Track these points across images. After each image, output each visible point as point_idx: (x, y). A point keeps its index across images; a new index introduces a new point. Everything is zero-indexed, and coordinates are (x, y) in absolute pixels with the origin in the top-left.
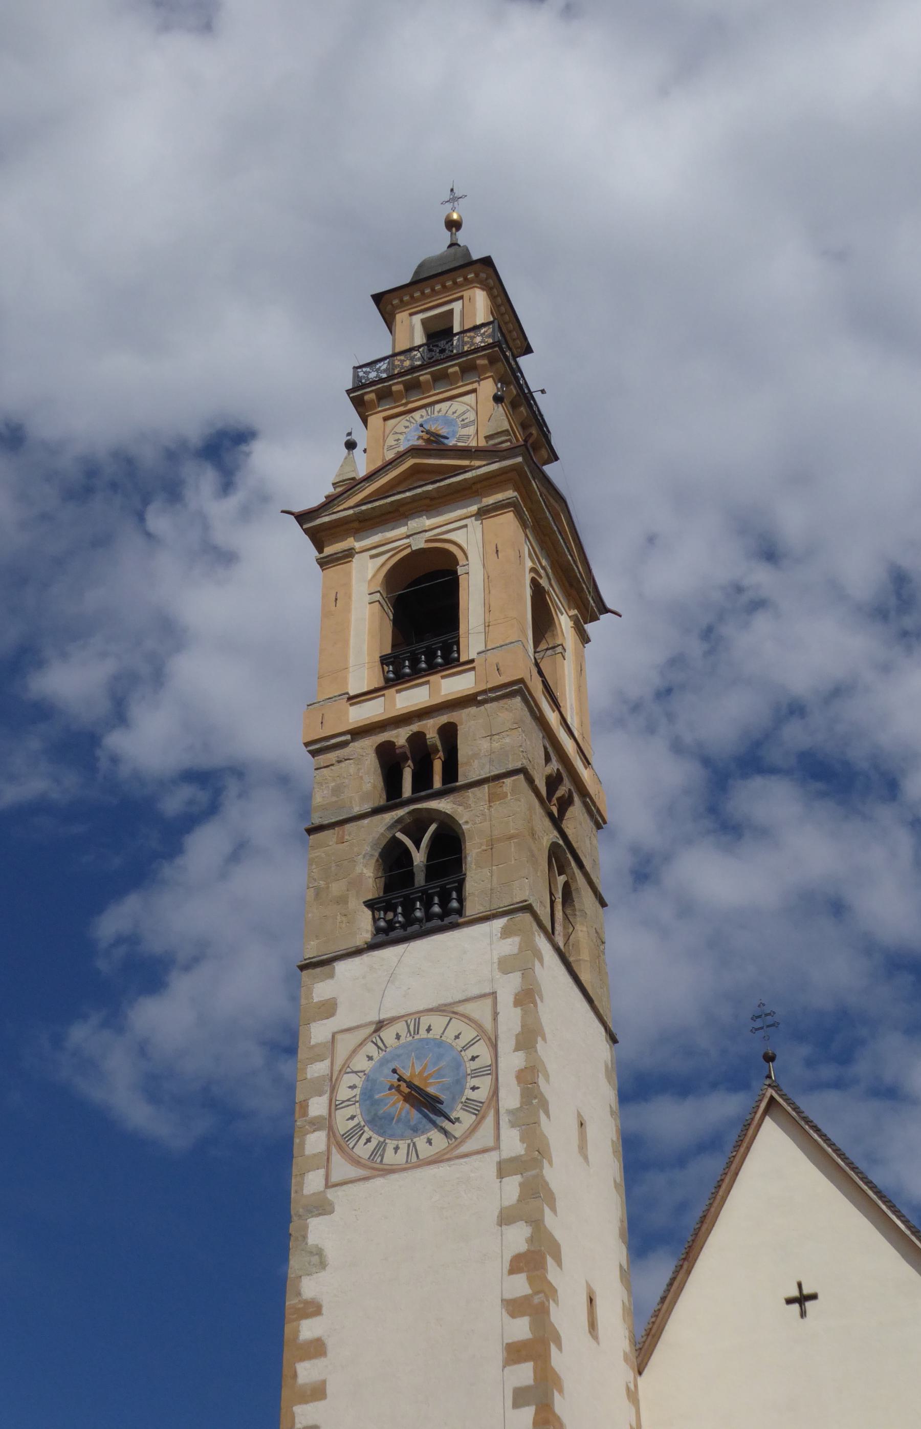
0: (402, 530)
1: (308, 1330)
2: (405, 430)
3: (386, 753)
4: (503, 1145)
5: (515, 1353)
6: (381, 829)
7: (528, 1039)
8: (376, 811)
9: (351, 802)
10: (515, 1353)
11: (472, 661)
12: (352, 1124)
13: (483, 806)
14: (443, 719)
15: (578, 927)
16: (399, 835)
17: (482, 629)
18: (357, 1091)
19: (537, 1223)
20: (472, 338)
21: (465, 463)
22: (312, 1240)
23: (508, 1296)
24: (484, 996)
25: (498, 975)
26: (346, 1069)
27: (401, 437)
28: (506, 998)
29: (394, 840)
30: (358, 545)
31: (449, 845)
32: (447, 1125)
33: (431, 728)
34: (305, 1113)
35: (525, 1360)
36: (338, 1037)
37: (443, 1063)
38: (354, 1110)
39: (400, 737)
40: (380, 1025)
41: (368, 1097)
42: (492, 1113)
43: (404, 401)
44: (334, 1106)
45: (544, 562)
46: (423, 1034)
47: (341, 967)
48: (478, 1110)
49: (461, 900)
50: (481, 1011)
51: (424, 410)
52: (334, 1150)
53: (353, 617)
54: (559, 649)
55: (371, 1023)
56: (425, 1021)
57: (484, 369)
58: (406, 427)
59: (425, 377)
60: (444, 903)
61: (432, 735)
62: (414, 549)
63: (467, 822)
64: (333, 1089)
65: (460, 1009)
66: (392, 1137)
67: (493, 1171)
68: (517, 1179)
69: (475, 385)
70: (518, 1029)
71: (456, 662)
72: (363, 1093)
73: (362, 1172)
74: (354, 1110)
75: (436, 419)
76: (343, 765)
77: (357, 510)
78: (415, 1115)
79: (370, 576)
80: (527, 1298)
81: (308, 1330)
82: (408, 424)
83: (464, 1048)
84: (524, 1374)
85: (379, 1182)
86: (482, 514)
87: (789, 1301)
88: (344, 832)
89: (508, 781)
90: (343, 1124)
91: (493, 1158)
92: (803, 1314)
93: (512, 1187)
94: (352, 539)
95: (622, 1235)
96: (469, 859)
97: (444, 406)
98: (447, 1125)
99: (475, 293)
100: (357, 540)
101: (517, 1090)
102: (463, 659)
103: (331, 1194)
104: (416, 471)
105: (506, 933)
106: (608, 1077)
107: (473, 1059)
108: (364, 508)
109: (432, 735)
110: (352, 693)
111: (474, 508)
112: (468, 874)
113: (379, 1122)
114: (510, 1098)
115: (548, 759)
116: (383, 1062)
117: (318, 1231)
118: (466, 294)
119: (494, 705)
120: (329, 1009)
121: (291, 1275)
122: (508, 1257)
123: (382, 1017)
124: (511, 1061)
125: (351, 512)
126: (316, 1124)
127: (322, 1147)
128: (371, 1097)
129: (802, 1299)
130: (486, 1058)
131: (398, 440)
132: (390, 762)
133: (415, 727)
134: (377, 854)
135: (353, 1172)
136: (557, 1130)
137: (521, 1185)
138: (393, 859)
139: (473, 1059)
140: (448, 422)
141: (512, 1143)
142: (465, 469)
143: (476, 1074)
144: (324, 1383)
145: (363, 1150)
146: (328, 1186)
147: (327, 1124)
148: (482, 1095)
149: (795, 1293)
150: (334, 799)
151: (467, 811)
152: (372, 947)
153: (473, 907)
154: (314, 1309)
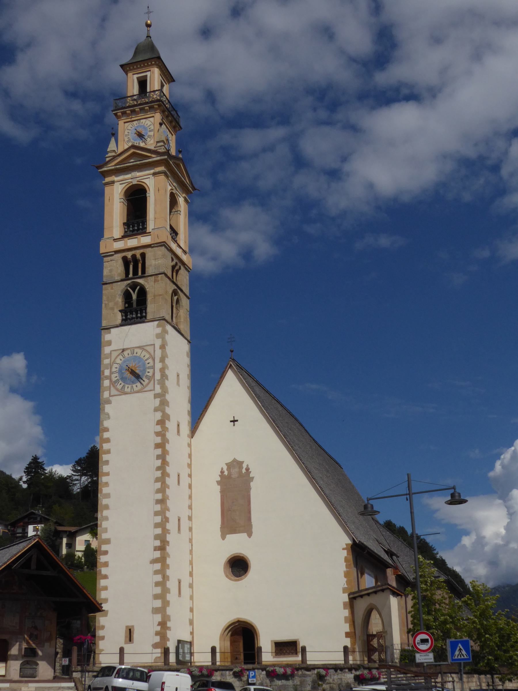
0: (129, 176)
1: (106, 435)
3: (125, 259)
4: (156, 389)
5: (157, 446)
6: (124, 287)
7: (162, 360)
8: (122, 280)
10: (157, 446)
11: (150, 233)
12: (116, 379)
13: (152, 283)
14: (141, 251)
15: (181, 311)
16: (129, 288)
17: (153, 219)
18: (117, 369)
19: (163, 412)
20: (153, 95)
21: (149, 155)
22: (106, 411)
23: (156, 431)
24: (152, 345)
25: (155, 339)
26: (114, 362)
27: (130, 131)
28: (157, 346)
30: (116, 179)
31: (143, 293)
32: (142, 381)
33: (138, 253)
34: (103, 374)
35: (159, 448)
36: (112, 352)
37: (140, 364)
38: (117, 375)
39: (129, 255)
40: (123, 350)
41: (120, 371)
42: (153, 380)
44: (111, 373)
45: (175, 184)
46: (135, 354)
47: (112, 330)
48: (149, 378)
49: (146, 313)
50: (150, 349)
52: (111, 386)
53: (115, 207)
54: (179, 212)
55: (120, 349)
56: (136, 350)
57: (156, 109)
59: (137, 109)
60: (141, 313)
61: (138, 256)
64: (111, 368)
65: (145, 348)
66: (127, 384)
67: (153, 396)
68: (159, 399)
69: (154, 115)
70: (160, 356)
71: (145, 233)
72: (119, 370)
73: (119, 393)
74: (117, 375)
75: (141, 126)
77: (115, 167)
78: (133, 378)
80: (160, 432)
81: (106, 435)
83: (146, 360)
84: (159, 451)
85: (123, 396)
86: (154, 174)
87: (231, 421)
90: (114, 379)
91: (152, 393)
92: (234, 425)
93: (158, 401)
94: (114, 176)
95: (189, 402)
97: (144, 121)
98: (142, 381)
100: (116, 177)
101: (160, 374)
102: (148, 231)
103: (111, 398)
104: (134, 154)
105: (158, 326)
106: (188, 356)
107: (148, 363)
108: (118, 167)
110: (115, 238)
111: (152, 171)
113: (123, 379)
114: (158, 376)
115: (173, 260)
116: (124, 362)
117: (108, 408)
118: (152, 69)
120: (109, 343)
121: (101, 420)
122: (156, 421)
123: (125, 347)
124: (158, 366)
125: (113, 167)
126: (107, 378)
127: (108, 385)
128: (121, 371)
129: (234, 421)
130: (151, 364)
132: (126, 262)
133: (133, 252)
135: (116, 393)
136: (170, 383)
137: (160, 401)
138: (127, 296)
139: (148, 363)
140: (145, 128)
141: (158, 389)
142: (149, 157)
143: (149, 368)
144: (110, 449)
145: (119, 387)
146: (110, 396)
147: (109, 378)
148: (150, 374)
149: (232, 419)
151: (148, 284)
152: (121, 325)
153: (149, 317)
154: (107, 430)
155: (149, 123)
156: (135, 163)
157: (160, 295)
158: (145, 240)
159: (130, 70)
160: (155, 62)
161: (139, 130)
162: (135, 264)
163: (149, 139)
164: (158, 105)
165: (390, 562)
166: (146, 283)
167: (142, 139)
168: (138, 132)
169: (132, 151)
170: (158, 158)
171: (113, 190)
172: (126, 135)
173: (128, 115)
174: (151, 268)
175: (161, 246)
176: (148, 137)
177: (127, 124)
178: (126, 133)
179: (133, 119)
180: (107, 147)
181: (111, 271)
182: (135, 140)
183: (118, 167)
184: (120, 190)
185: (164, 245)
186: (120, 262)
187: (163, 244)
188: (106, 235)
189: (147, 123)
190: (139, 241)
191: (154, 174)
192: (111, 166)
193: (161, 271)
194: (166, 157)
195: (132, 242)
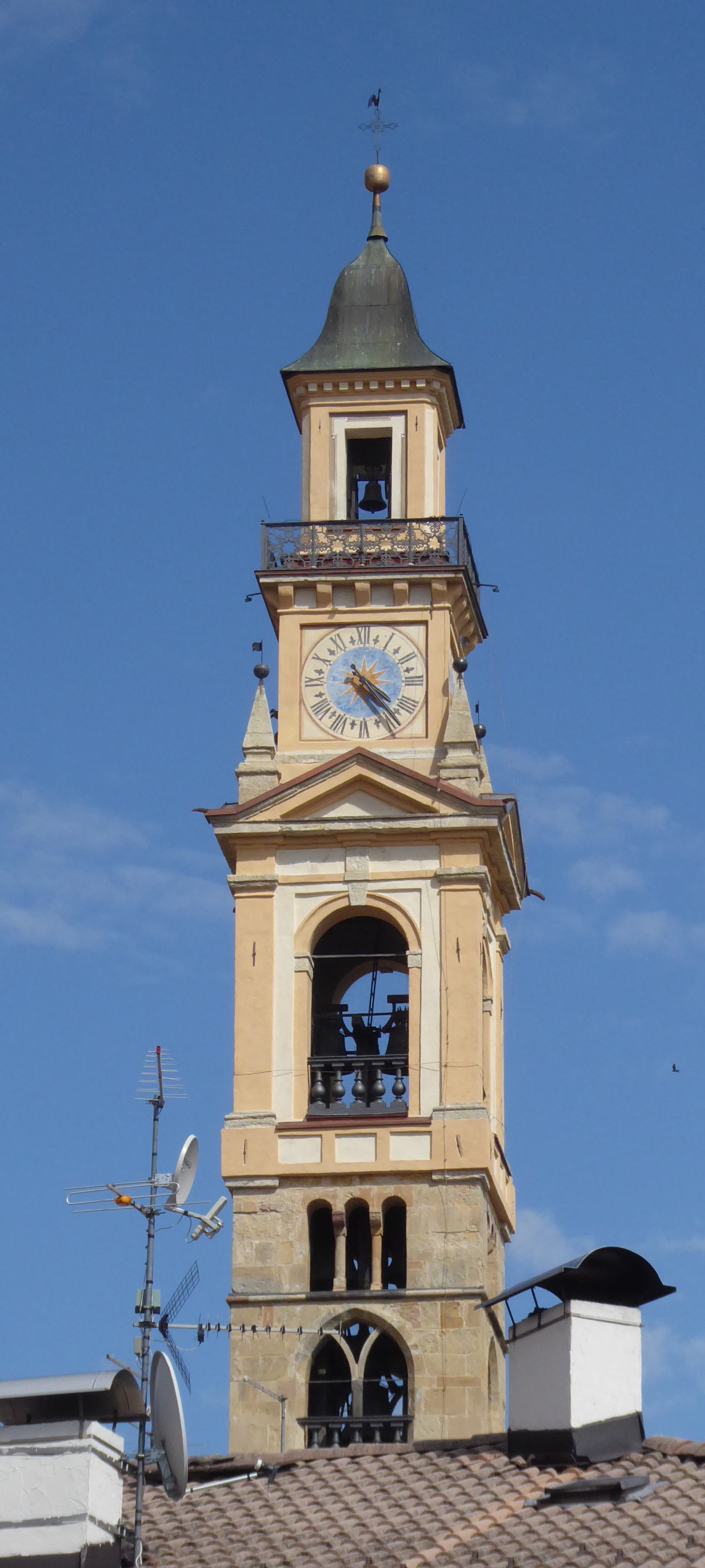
2: (330, 658)
3: (319, 1214)
9: (280, 1275)
13: (434, 1329)
14: (390, 1190)
27: (325, 668)
29: (329, 1337)
31: (391, 1355)
33: (375, 1197)
39: (339, 1199)
43: (329, 608)
51: (354, 629)
53: (276, 990)
57: (441, 596)
58: (332, 653)
59: (362, 583)
61: (376, 1211)
62: (353, 903)
63: (416, 1346)
69: (425, 616)
75: (372, 654)
76: (266, 1215)
77: (286, 827)
79: (295, 931)
82: (333, 647)
86: (440, 880)
88: (272, 1315)
89: (465, 1303)
94: (271, 860)
96: (417, 1396)
99: (423, 413)
100: (281, 861)
102: (412, 1114)
104: (360, 781)
108: (295, 827)
109: (376, 1211)
112: (416, 1415)
119: (451, 1188)
125: (276, 828)
131: (320, 672)
133: (355, 1191)
134: (309, 1355)
138: (327, 1360)
140: (389, 667)
142: (428, 812)
150: (259, 1264)
151: (417, 1329)
155: (407, 649)
156: (366, 825)
157: (465, 1382)
158: (406, 1150)
159: (322, 394)
160: (428, 382)
161: (366, 668)
162: (357, 1240)
163: (404, 716)
164: (450, 583)
165: (140, 1386)
166: (408, 1325)
167: (375, 712)
168: (362, 679)
169: (355, 770)
170: (463, 822)
171: (269, 917)
172: (310, 683)
173: (321, 600)
174: (427, 1267)
175: (472, 1182)
176: (401, 705)
177: (312, 635)
178: (309, 671)
179: (339, 618)
180: (242, 732)
181: (263, 1252)
182: (348, 710)
183: (295, 827)
184: (296, 925)
185: (481, 1181)
186: (301, 1223)
187: (480, 1178)
188: (244, 1104)
189: (402, 643)
190: (379, 1151)
191: (440, 880)
192: (265, 822)
193: (472, 1284)
194: (494, 822)
195: (353, 1151)
